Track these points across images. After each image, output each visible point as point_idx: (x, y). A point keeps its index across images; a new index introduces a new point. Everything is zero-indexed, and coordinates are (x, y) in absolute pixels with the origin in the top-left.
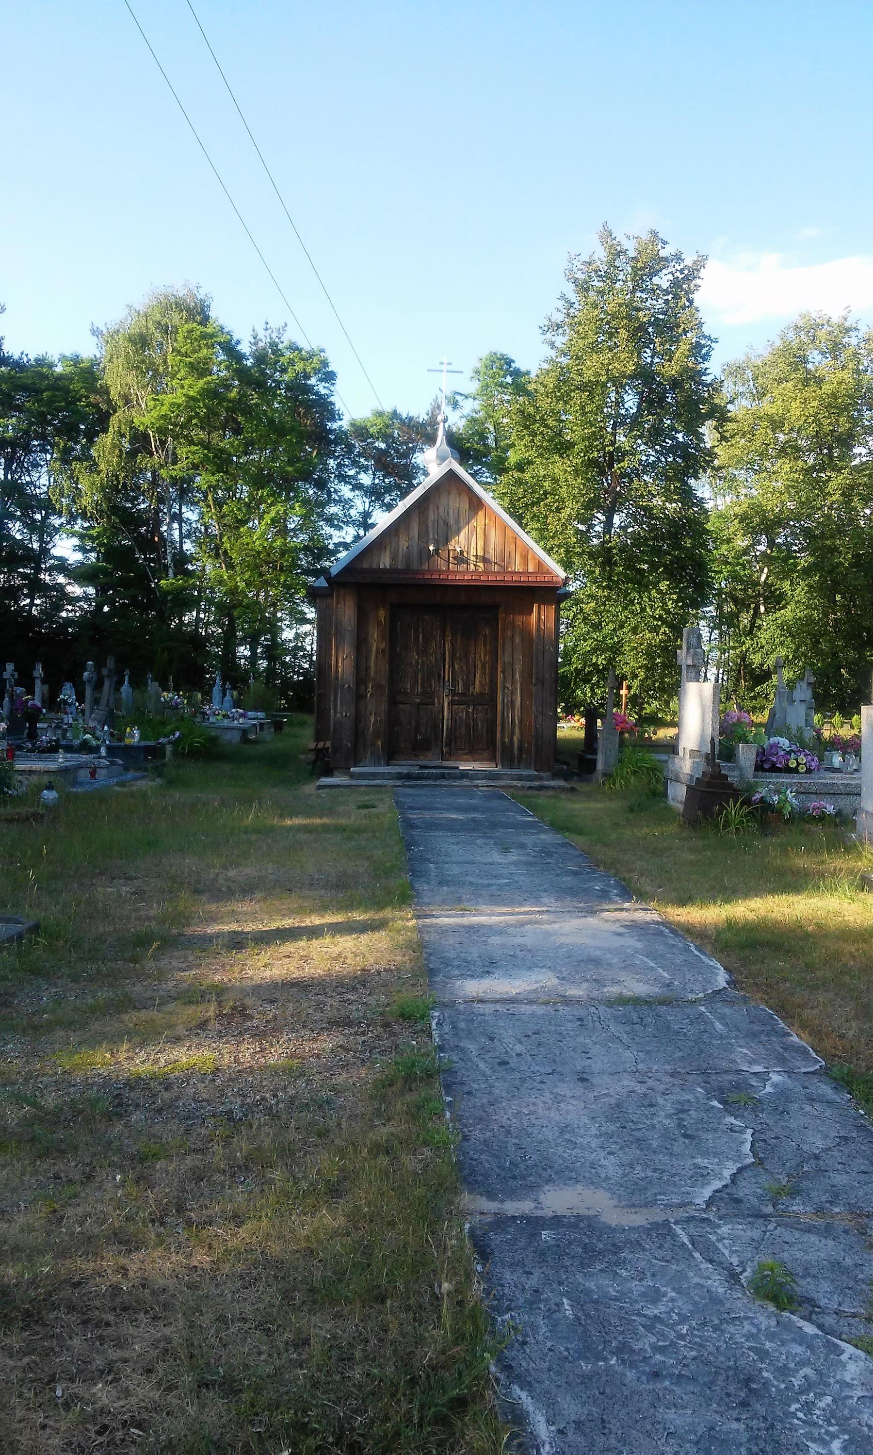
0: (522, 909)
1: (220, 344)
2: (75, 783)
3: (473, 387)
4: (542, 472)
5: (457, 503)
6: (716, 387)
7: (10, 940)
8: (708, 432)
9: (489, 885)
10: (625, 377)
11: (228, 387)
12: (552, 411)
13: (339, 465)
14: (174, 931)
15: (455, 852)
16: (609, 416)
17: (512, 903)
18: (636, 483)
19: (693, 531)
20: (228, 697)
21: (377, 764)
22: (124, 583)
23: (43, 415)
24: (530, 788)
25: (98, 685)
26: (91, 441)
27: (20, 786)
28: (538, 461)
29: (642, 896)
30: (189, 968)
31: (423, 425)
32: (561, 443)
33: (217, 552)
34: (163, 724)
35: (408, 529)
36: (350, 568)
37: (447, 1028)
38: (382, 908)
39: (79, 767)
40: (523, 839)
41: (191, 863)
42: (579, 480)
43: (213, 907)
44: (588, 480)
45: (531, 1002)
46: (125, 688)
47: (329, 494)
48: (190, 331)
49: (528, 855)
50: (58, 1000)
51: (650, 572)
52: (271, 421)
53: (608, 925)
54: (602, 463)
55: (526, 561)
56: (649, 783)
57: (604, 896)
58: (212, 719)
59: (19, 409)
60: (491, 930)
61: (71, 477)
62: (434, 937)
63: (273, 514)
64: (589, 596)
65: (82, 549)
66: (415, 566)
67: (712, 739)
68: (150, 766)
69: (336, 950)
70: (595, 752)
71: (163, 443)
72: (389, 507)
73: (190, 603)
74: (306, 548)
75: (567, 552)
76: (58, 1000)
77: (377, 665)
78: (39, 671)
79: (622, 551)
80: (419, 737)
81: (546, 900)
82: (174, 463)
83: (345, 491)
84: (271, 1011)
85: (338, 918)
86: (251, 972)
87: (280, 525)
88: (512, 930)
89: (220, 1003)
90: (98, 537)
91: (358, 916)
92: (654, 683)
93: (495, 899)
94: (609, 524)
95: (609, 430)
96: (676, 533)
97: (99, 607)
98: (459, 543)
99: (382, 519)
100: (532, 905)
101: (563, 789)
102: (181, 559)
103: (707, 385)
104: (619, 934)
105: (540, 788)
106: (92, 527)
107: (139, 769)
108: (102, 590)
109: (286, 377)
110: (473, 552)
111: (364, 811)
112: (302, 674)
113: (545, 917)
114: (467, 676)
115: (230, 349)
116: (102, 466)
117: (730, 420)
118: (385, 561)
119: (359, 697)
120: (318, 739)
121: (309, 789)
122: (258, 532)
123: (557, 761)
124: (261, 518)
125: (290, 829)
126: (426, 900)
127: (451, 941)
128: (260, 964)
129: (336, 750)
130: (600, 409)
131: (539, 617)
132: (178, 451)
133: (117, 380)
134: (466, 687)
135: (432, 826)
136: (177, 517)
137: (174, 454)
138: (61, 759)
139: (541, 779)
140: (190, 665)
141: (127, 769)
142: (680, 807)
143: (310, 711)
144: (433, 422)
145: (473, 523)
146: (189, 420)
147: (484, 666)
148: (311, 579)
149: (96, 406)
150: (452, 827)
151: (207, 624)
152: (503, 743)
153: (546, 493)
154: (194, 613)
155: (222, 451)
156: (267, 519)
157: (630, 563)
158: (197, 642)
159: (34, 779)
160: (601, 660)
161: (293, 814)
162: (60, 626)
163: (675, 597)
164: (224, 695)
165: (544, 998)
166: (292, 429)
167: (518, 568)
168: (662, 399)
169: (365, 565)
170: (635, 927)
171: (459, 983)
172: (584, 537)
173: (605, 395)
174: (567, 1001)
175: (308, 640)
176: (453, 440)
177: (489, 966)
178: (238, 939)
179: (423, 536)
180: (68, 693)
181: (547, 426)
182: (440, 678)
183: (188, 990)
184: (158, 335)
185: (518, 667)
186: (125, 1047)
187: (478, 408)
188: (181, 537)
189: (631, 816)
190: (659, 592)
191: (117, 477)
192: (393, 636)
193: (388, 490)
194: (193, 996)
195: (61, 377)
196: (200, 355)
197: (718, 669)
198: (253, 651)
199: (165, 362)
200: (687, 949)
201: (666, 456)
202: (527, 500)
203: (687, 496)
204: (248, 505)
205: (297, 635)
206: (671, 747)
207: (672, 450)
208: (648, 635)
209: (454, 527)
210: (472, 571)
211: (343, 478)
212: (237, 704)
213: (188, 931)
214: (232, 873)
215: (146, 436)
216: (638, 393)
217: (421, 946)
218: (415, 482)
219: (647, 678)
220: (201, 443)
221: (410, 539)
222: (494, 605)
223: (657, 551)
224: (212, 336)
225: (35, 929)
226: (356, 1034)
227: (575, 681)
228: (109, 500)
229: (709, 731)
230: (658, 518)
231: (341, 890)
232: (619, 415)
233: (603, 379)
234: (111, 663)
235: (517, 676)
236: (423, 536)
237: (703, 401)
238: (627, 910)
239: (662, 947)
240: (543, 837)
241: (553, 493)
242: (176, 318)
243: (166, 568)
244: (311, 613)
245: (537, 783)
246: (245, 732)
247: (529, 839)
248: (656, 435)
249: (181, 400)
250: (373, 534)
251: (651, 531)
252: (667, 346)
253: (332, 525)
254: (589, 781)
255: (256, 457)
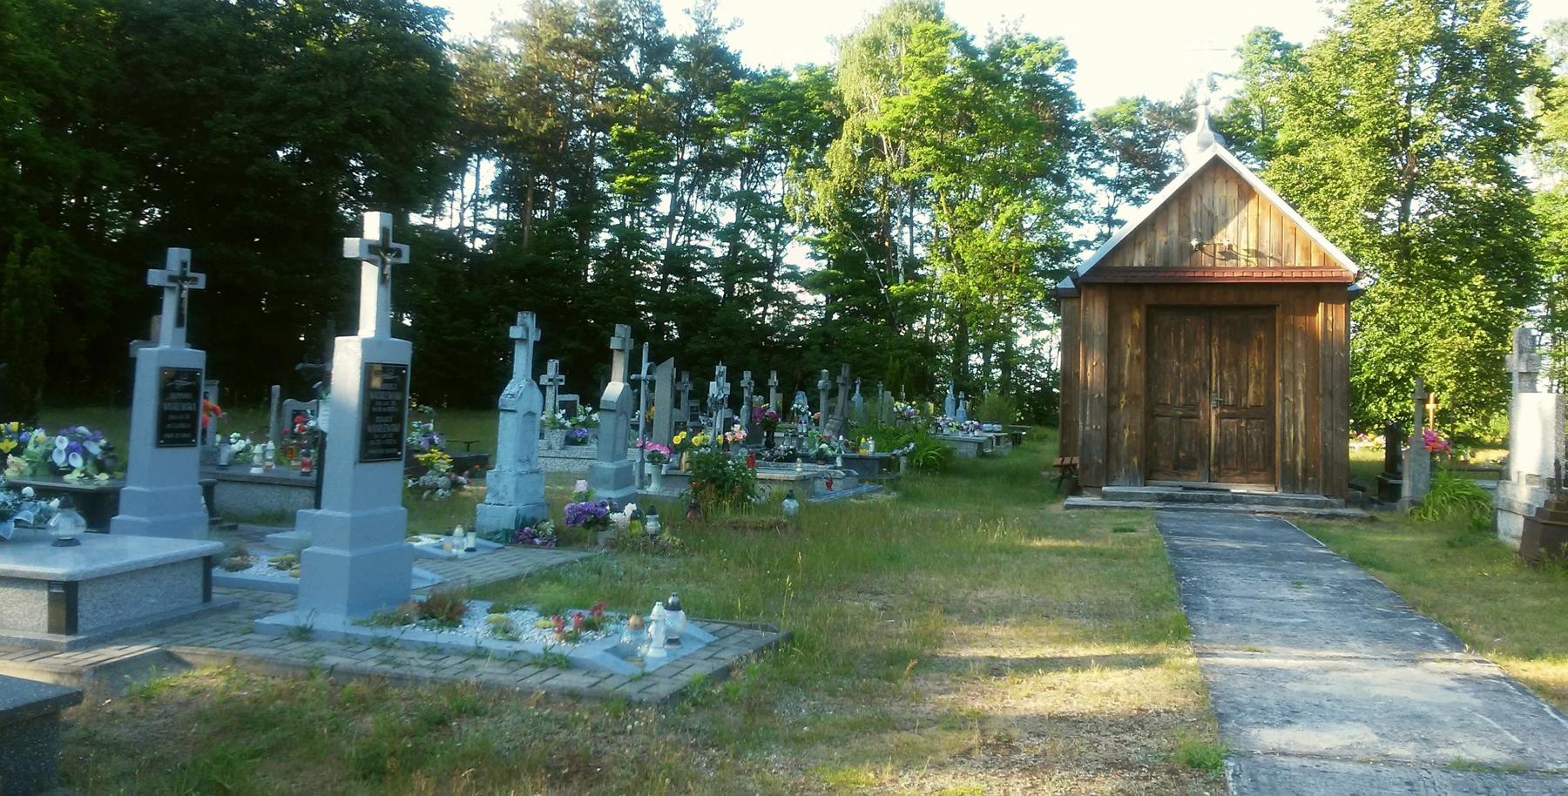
0: (1324, 653)
1: (954, 40)
2: (813, 494)
3: (1237, 64)
4: (1321, 155)
5: (1222, 193)
6: (1536, 49)
7: (769, 646)
8: (1528, 99)
9: (1280, 624)
10: (1420, 43)
11: (961, 85)
12: (1332, 86)
13: (1081, 159)
14: (927, 652)
15: (1234, 585)
16: (1403, 88)
17: (1310, 645)
18: (1438, 163)
19: (1515, 216)
20: (961, 408)
21: (1133, 483)
22: (854, 291)
23: (778, 124)
24: (1319, 516)
25: (833, 393)
26: (824, 149)
27: (762, 494)
28: (1315, 142)
29: (1477, 646)
30: (947, 691)
31: (1176, 110)
32: (1343, 121)
33: (948, 255)
34: (896, 435)
35: (1166, 221)
36: (1099, 268)
37: (1245, 781)
38: (1155, 643)
39: (816, 478)
40: (1316, 573)
41: (937, 581)
42: (1367, 162)
43: (965, 629)
44: (1378, 161)
45: (1345, 760)
46: (857, 397)
47: (1069, 189)
48: (924, 31)
49: (1325, 592)
50: (817, 714)
51: (1459, 264)
52: (1007, 117)
53: (1435, 677)
54: (1395, 141)
55: (1308, 255)
56: (1471, 514)
57: (1426, 642)
58: (946, 431)
59: (756, 119)
60: (1288, 674)
61: (804, 185)
62: (1219, 678)
63: (1008, 213)
64: (1384, 294)
65: (815, 257)
66: (1174, 263)
67: (1557, 463)
68: (885, 478)
69: (1106, 685)
70: (1399, 476)
71: (895, 146)
72: (1138, 201)
73: (922, 309)
74: (1044, 248)
75: (1354, 244)
76: (817, 714)
77: (1131, 373)
78: (774, 380)
79: (1422, 240)
80: (1182, 454)
81: (1353, 645)
82: (906, 166)
83: (1087, 185)
84: (1040, 745)
85: (1106, 650)
86: (1013, 702)
87: (1015, 224)
88: (1313, 676)
89: (983, 731)
90: (830, 243)
91: (1128, 650)
92: (1467, 396)
93: (1290, 641)
94: (1404, 211)
95: (1403, 103)
96: (1493, 218)
97: (829, 314)
98: (1225, 237)
99: (1133, 216)
100: (1336, 649)
101: (1361, 519)
102: (912, 264)
103: (1525, 47)
104: (1449, 689)
105: (1332, 516)
106: (824, 234)
107: (874, 481)
108: (831, 299)
109: (1023, 70)
110: (1244, 246)
111: (1121, 535)
112: (1037, 385)
113: (1353, 663)
114: (1239, 384)
115: (964, 45)
116: (835, 173)
117: (1556, 85)
118: (1139, 259)
119: (1111, 408)
120: (1063, 455)
121: (1056, 508)
122: (992, 234)
123: (1351, 486)
124: (996, 218)
125: (1039, 550)
126: (1207, 637)
127: (1241, 684)
128: (1023, 694)
129: (1085, 467)
130: (1389, 80)
131: (1327, 318)
132: (911, 153)
133: (851, 85)
134: (1237, 397)
135: (1203, 554)
136: (907, 221)
137: (906, 156)
138: (799, 469)
139: (1332, 506)
140: (917, 374)
141: (862, 481)
142: (1517, 544)
143: (1053, 425)
144: (1190, 105)
145: (1243, 213)
146: (922, 120)
147: (1258, 374)
148: (1048, 281)
149: (829, 112)
150: (1228, 557)
151: (938, 331)
152: (1284, 464)
153: (1325, 178)
154: (924, 320)
155: (955, 150)
156: (1002, 218)
157: (1433, 256)
158: (927, 350)
159: (775, 488)
160: (1399, 369)
161: (1043, 534)
162: (791, 334)
163: (1493, 293)
164: (957, 406)
165: (1361, 756)
166: (1030, 123)
167: (1300, 262)
168: (1467, 66)
169: (1117, 264)
170: (1467, 680)
171: (1254, 732)
172: (1373, 226)
173: (1395, 64)
174: (1390, 761)
175: (1046, 347)
176: (1216, 125)
177: (1290, 715)
178: (996, 665)
179: (1184, 230)
180: (800, 402)
181: (1325, 103)
182: (1205, 387)
183: (947, 716)
184: (891, 37)
185: (1301, 375)
186: (889, 768)
187: (1241, 87)
188: (912, 242)
189: (1451, 552)
190: (1473, 288)
191: (849, 183)
192: (1149, 340)
193: (1136, 182)
194: (954, 722)
195: (796, 86)
196: (934, 53)
197: (1551, 379)
198: (986, 358)
199: (898, 64)
200: (1540, 711)
201: (1474, 129)
202: (1305, 186)
203: (1503, 175)
204: (981, 205)
205: (1034, 343)
206: (1500, 472)
207: (1482, 123)
208: (1459, 339)
209: (1220, 219)
210: (1244, 267)
211: (1083, 172)
212: (971, 415)
213: (942, 653)
214: (981, 595)
215: (877, 140)
216: (1437, 61)
217: (1206, 687)
218: (1167, 173)
219: (1458, 390)
220: (934, 144)
221: (1168, 233)
222: (1266, 307)
223: (1468, 240)
224: (947, 33)
225: (790, 638)
226: (1137, 778)
227: (1367, 395)
228: (842, 206)
229: (1552, 454)
230: (1466, 202)
231: (1106, 619)
232: (1413, 87)
233: (1393, 47)
234: (845, 371)
235: (1300, 387)
236: (1184, 230)
237: (1521, 65)
238: (1457, 661)
239: (1508, 707)
240: (1341, 572)
241: (1335, 177)
242: (910, 18)
243: (897, 272)
244: (1048, 318)
245: (1327, 511)
246: (980, 445)
247: (1325, 574)
248: (1461, 106)
249: (915, 101)
250: (1119, 234)
251: (1459, 217)
252: (1472, 5)
253: (1072, 223)
254: (1393, 509)
255: (991, 155)
